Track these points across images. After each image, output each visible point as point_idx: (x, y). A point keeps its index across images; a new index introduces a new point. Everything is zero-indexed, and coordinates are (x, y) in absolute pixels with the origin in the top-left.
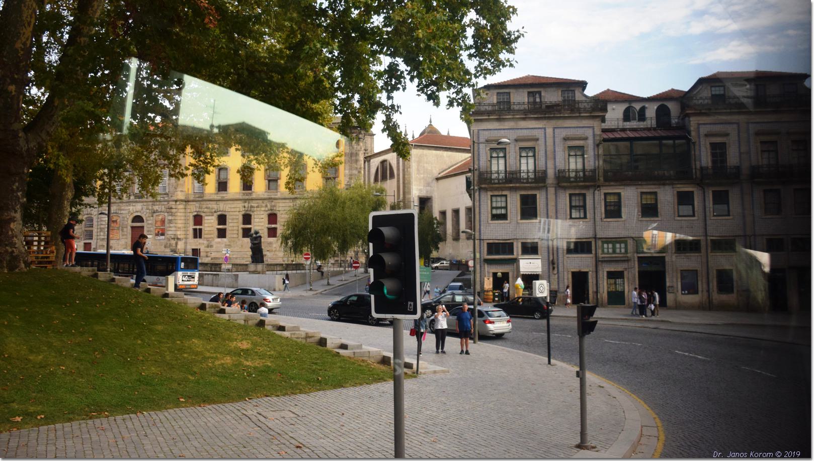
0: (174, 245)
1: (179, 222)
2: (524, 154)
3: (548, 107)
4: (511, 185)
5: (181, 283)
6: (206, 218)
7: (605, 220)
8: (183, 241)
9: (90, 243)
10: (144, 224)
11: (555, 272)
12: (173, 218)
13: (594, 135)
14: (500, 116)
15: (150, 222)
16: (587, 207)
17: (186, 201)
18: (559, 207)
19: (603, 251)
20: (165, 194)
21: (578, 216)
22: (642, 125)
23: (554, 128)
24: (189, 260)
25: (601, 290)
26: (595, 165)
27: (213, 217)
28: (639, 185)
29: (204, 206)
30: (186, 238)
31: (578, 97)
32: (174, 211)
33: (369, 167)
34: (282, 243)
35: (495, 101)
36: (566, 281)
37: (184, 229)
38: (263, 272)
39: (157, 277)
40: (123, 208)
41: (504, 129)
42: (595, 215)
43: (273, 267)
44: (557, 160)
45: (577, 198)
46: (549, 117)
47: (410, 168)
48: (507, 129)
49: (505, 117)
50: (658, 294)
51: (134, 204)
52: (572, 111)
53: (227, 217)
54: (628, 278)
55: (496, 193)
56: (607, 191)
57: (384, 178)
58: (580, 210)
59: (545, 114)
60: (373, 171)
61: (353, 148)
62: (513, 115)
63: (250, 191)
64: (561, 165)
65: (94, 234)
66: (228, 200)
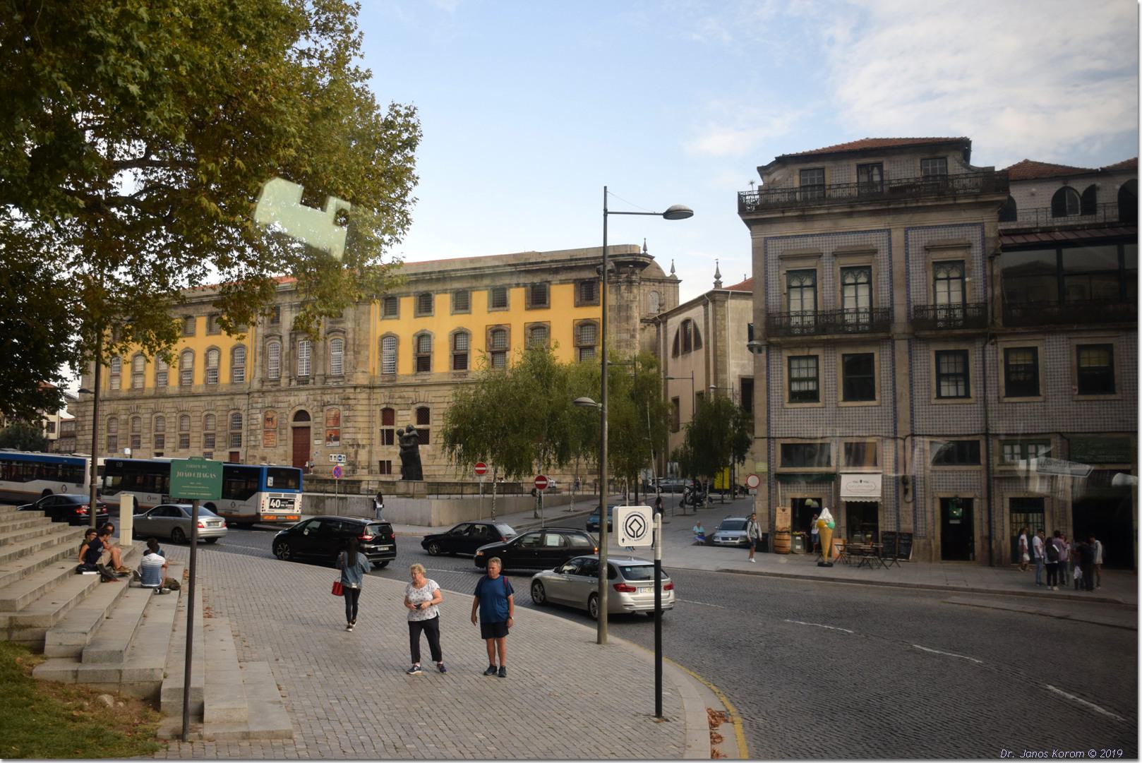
0: (352, 455)
1: (360, 419)
2: (850, 280)
3: (893, 190)
4: (825, 337)
5: (267, 510)
6: (400, 412)
7: (1006, 400)
8: (367, 449)
9: (238, 452)
10: (311, 423)
11: (909, 498)
12: (351, 413)
13: (984, 240)
14: (803, 210)
15: (318, 420)
16: (971, 375)
17: (370, 388)
18: (915, 379)
19: (1002, 458)
20: (339, 377)
21: (953, 393)
22: (1087, 220)
23: (907, 230)
24: (283, 474)
25: (998, 534)
26: (985, 297)
27: (410, 412)
28: (1076, 331)
29: (397, 395)
30: (371, 445)
31: (953, 167)
32: (352, 402)
33: (665, 331)
34: (444, 447)
35: (797, 184)
36: (929, 515)
37: (367, 430)
38: (422, 496)
39: (232, 501)
40: (280, 399)
41: (812, 235)
42: (985, 391)
43: (437, 488)
44: (912, 289)
45: (952, 359)
46: (897, 209)
47: (725, 330)
48: (817, 235)
49: (812, 213)
50: (1102, 543)
51: (296, 393)
52: (941, 194)
53: (431, 411)
54: (1052, 513)
55: (798, 353)
56: (1009, 345)
57: (687, 349)
58: (957, 382)
59: (889, 204)
60: (671, 337)
61: (622, 297)
62: (829, 208)
63: (464, 371)
64: (919, 296)
65: (244, 438)
66: (431, 385)
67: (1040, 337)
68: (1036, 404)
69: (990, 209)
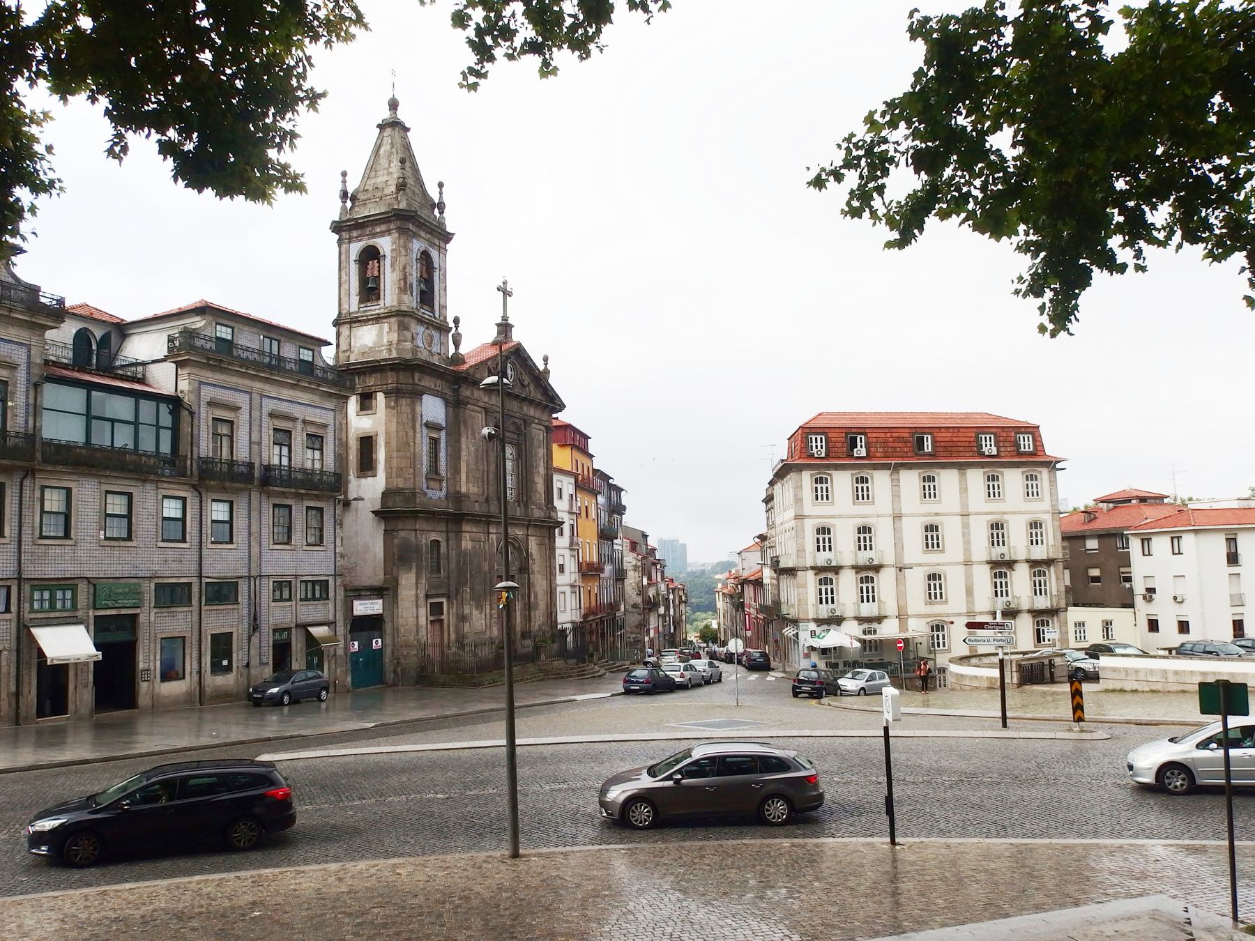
13: (29, 364)
67: (74, 477)
68: (67, 547)
69: (38, 332)
